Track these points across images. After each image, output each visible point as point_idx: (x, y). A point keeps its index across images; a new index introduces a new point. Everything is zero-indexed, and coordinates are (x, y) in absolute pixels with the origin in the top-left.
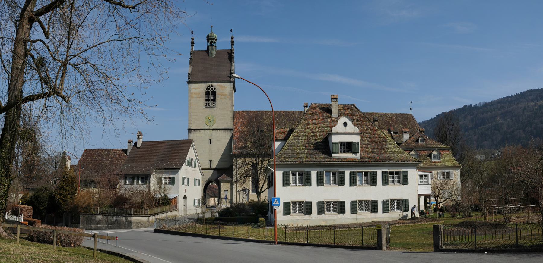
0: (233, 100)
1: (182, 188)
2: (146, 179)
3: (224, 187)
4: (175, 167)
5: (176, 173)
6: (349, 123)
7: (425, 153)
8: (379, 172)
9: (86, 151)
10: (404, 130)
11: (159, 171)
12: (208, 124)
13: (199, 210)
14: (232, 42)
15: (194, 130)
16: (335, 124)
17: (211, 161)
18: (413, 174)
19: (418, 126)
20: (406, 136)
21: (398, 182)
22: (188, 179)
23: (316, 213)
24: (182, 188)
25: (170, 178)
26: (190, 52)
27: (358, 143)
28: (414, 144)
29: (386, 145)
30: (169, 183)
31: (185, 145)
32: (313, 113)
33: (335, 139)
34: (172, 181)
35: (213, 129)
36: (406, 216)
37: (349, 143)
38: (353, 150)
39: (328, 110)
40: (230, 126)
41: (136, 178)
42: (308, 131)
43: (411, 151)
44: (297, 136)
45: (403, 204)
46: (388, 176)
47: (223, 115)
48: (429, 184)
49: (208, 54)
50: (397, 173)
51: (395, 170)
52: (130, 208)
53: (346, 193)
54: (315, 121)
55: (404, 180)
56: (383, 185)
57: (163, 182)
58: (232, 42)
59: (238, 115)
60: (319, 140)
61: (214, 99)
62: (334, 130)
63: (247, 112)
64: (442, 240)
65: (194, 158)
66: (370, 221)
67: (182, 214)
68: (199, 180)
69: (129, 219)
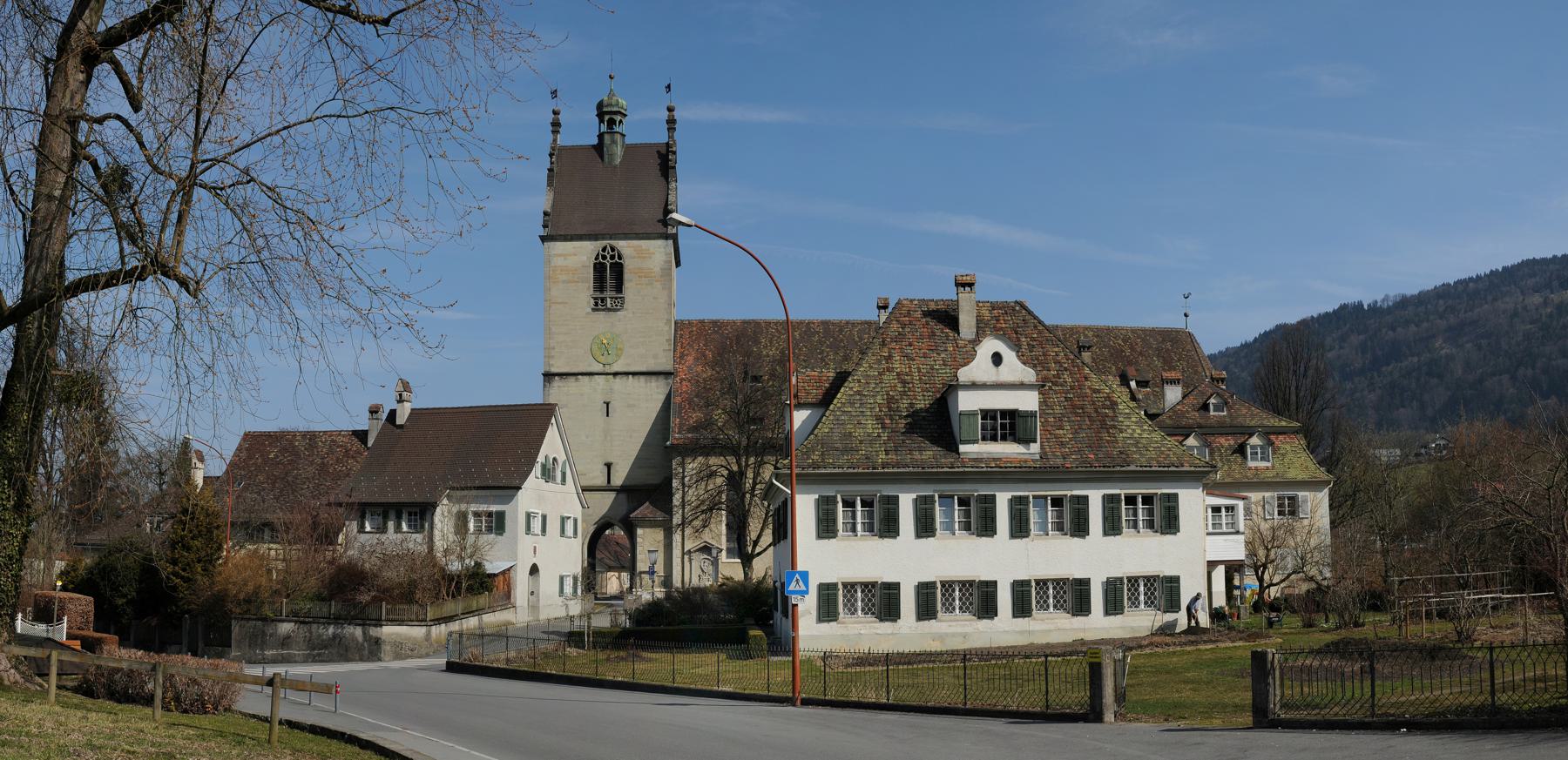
0: (674, 290)
1: (525, 543)
2: (423, 519)
3: (648, 540)
4: (504, 482)
5: (509, 500)
6: (1009, 356)
7: (1227, 442)
8: (1095, 497)
9: (248, 436)
10: (1165, 375)
11: (459, 493)
12: (602, 359)
13: (576, 608)
14: (671, 122)
15: (561, 375)
16: (969, 358)
17: (609, 466)
18: (1193, 502)
19: (1208, 364)
20: (1173, 394)
21: (1150, 525)
22: (544, 518)
23: (913, 616)
24: (525, 543)
25: (490, 514)
26: (548, 150)
27: (1032, 414)
28: (1195, 417)
29: (1114, 418)
30: (489, 530)
31: (535, 419)
32: (904, 326)
33: (967, 402)
34: (497, 524)
35: (615, 374)
36: (1174, 624)
37: (1007, 414)
38: (1020, 433)
39: (947, 318)
40: (665, 363)
41: (392, 515)
42: (889, 378)
43: (1187, 436)
44: (858, 393)
45: (1165, 590)
46: (1119, 509)
47: (643, 333)
48: (1238, 533)
49: (602, 156)
50: (1148, 500)
51: (1139, 490)
52: (377, 601)
53: (1000, 559)
54: (909, 350)
55: (1168, 521)
56: (1105, 534)
57: (471, 526)
58: (671, 122)
59: (688, 333)
60: (921, 404)
61: (619, 287)
62: (965, 374)
63: (715, 323)
64: (1276, 695)
65: (562, 458)
66: (1068, 638)
67: (527, 619)
68: (575, 520)
69: (374, 631)
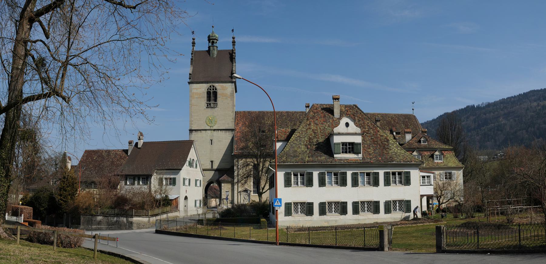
1: (183, 189)
2: (147, 180)
3: (226, 188)
4: (176, 168)
5: (177, 174)
6: (351, 124)
7: (427, 154)
8: (381, 173)
9: (86, 152)
10: (406, 130)
11: (160, 171)
12: (210, 125)
13: (200, 211)
14: (234, 42)
15: (195, 130)
16: (337, 124)
17: (212, 162)
18: (415, 175)
19: (421, 127)
20: (408, 137)
21: (401, 182)
22: (190, 180)
23: (318, 214)
24: (183, 189)
25: (171, 179)
26: (191, 52)
27: (360, 144)
28: (416, 145)
29: (388, 145)
30: (170, 184)
31: (186, 146)
32: (315, 113)
33: (337, 139)
34: (173, 182)
35: (214, 130)
36: (409, 217)
37: (351, 144)
38: (355, 150)
39: (330, 110)
40: (232, 126)
41: (137, 179)
42: (310, 131)
43: (413, 151)
44: (299, 136)
45: (406, 205)
46: (390, 177)
47: (224, 116)
48: (431, 185)
49: (209, 54)
50: (400, 174)
51: (397, 170)
52: (131, 209)
53: (348, 194)
54: (316, 122)
55: (407, 181)
56: (385, 185)
57: (164, 183)
58: (234, 42)
59: (239, 116)
60: (321, 140)
61: (215, 100)
62: (336, 130)
63: (249, 112)
65: (196, 159)
66: (372, 222)
67: (183, 215)
68: (200, 181)
69: (130, 219)
